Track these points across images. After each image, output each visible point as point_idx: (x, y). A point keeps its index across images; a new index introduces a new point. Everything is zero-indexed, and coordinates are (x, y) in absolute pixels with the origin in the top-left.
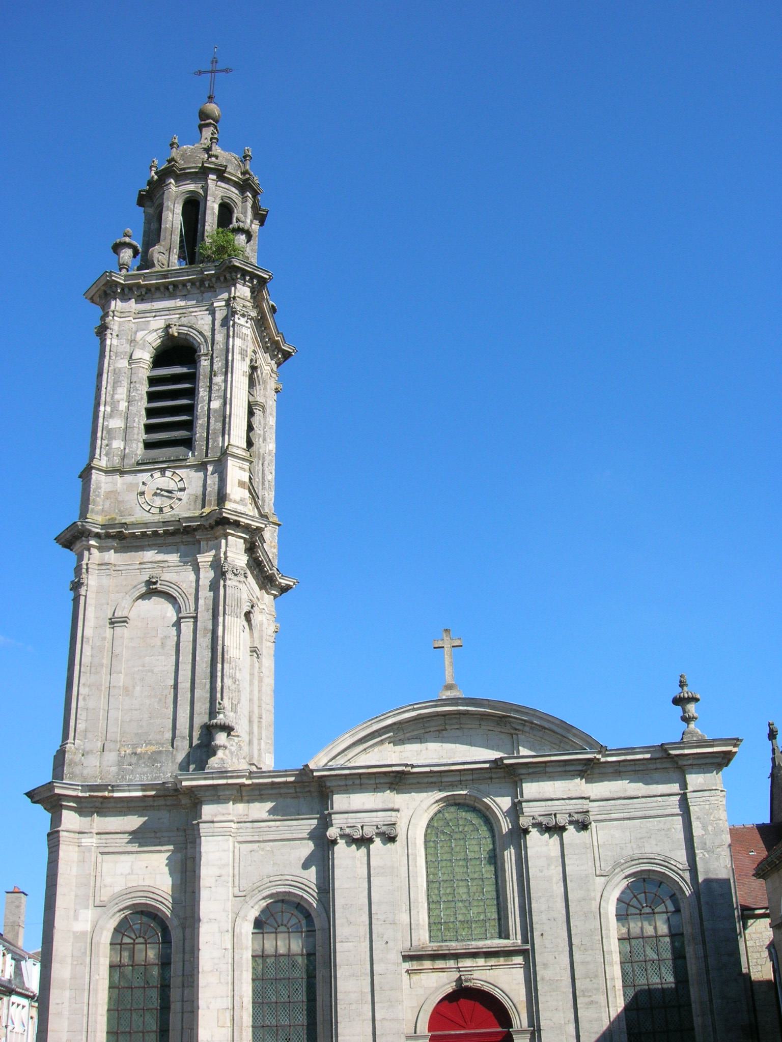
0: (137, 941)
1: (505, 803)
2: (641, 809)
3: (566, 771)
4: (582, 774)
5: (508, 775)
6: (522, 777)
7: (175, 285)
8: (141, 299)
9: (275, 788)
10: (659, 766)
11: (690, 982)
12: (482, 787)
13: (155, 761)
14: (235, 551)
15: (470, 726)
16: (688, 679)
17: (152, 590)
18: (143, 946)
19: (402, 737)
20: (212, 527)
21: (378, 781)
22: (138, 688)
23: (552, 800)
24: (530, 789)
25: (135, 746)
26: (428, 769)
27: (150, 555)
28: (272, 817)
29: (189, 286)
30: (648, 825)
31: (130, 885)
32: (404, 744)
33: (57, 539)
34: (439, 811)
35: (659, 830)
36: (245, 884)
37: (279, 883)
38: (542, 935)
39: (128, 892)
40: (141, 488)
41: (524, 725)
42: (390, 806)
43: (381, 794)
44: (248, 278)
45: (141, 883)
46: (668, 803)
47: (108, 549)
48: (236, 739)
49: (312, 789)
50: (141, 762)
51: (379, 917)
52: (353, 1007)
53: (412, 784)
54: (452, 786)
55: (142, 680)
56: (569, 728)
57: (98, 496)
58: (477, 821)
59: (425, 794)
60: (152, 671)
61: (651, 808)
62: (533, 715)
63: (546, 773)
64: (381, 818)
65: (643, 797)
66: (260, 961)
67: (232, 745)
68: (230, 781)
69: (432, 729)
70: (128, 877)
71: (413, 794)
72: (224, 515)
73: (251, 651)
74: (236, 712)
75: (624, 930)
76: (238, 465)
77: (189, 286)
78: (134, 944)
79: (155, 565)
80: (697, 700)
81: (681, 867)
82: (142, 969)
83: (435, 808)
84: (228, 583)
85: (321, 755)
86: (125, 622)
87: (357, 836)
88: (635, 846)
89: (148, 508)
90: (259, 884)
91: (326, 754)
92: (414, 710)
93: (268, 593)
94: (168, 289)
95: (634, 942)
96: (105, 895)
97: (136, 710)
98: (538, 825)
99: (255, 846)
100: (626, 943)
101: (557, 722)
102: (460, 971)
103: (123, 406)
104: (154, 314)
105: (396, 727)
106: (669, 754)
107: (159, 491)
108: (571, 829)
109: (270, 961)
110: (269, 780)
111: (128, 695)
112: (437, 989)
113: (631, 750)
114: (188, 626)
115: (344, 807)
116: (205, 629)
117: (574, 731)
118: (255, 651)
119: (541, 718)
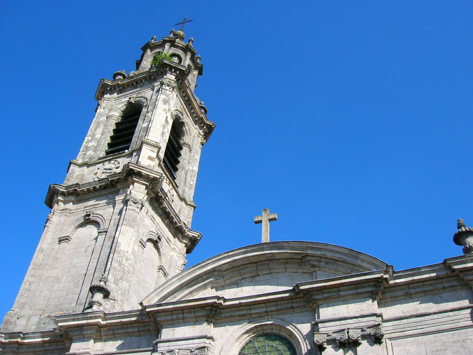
1: (306, 328)
3: (357, 294)
4: (373, 296)
5: (306, 302)
6: (320, 302)
8: (120, 92)
9: (124, 328)
10: (446, 285)
12: (286, 317)
14: (138, 191)
15: (277, 270)
17: (88, 221)
19: (223, 283)
21: (196, 314)
22: (65, 277)
23: (345, 319)
24: (326, 312)
26: (237, 302)
28: (119, 351)
30: (443, 338)
32: (224, 289)
34: (250, 342)
35: (454, 342)
41: (320, 261)
42: (204, 334)
43: (200, 326)
44: (173, 70)
46: (459, 317)
47: (69, 202)
48: (112, 301)
49: (151, 328)
53: (226, 317)
54: (260, 317)
56: (356, 254)
57: (72, 177)
58: (282, 347)
59: (237, 326)
62: (326, 250)
63: (340, 296)
65: (434, 313)
67: (107, 304)
68: (90, 321)
69: (247, 276)
71: (227, 326)
72: (130, 167)
73: (159, 269)
74: (117, 285)
76: (150, 149)
83: (246, 338)
84: (129, 207)
86: (67, 239)
92: (229, 257)
93: (181, 242)
98: (331, 342)
101: (347, 252)
105: (216, 273)
106: (454, 270)
107: (105, 171)
108: (364, 343)
110: (119, 320)
113: (416, 271)
114: (101, 237)
116: (111, 236)
117: (362, 257)
118: (161, 269)
119: (333, 251)
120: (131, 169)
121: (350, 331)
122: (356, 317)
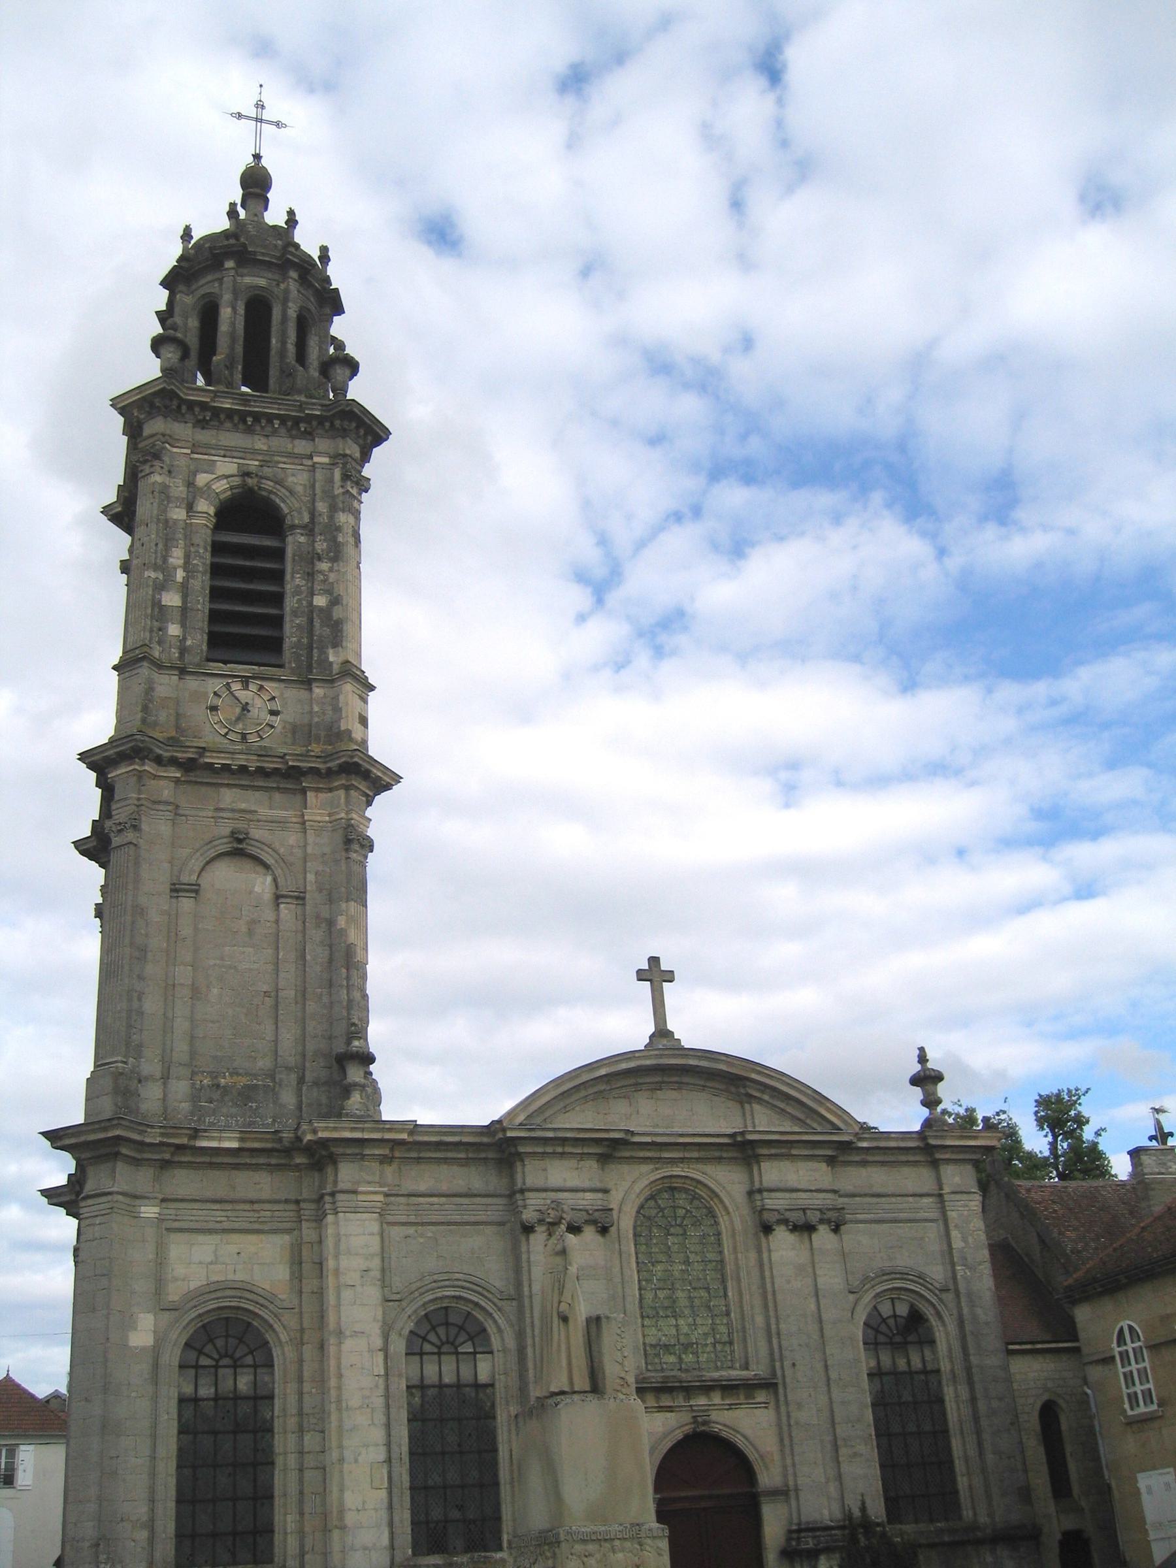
0: (221, 1363)
3: (211, 1163)
7: (257, 417)
11: (952, 1432)
17: (239, 849)
18: (230, 1371)
20: (330, 773)
22: (215, 991)
25: (214, 1075)
27: (229, 797)
29: (276, 423)
31: (214, 1278)
33: (84, 757)
36: (397, 1282)
37: (447, 1283)
38: (794, 1365)
39: (244, 1289)
45: (231, 1277)
50: (227, 1098)
61: (901, 1211)
64: (589, 1200)
66: (417, 1393)
75: (873, 1363)
77: (276, 423)
78: (216, 1367)
79: (237, 815)
81: (938, 1285)
89: (223, 731)
90: (418, 1284)
94: (245, 422)
95: (886, 1379)
96: (174, 1293)
97: (212, 1022)
99: (411, 1230)
100: (877, 1380)
101: (810, 1092)
102: (693, 1411)
103: (180, 575)
104: (222, 453)
106: (928, 1144)
109: (431, 1392)
112: (665, 1435)
115: (540, 1183)
120: (293, 767)
121: (808, 1212)
122: (811, 1191)
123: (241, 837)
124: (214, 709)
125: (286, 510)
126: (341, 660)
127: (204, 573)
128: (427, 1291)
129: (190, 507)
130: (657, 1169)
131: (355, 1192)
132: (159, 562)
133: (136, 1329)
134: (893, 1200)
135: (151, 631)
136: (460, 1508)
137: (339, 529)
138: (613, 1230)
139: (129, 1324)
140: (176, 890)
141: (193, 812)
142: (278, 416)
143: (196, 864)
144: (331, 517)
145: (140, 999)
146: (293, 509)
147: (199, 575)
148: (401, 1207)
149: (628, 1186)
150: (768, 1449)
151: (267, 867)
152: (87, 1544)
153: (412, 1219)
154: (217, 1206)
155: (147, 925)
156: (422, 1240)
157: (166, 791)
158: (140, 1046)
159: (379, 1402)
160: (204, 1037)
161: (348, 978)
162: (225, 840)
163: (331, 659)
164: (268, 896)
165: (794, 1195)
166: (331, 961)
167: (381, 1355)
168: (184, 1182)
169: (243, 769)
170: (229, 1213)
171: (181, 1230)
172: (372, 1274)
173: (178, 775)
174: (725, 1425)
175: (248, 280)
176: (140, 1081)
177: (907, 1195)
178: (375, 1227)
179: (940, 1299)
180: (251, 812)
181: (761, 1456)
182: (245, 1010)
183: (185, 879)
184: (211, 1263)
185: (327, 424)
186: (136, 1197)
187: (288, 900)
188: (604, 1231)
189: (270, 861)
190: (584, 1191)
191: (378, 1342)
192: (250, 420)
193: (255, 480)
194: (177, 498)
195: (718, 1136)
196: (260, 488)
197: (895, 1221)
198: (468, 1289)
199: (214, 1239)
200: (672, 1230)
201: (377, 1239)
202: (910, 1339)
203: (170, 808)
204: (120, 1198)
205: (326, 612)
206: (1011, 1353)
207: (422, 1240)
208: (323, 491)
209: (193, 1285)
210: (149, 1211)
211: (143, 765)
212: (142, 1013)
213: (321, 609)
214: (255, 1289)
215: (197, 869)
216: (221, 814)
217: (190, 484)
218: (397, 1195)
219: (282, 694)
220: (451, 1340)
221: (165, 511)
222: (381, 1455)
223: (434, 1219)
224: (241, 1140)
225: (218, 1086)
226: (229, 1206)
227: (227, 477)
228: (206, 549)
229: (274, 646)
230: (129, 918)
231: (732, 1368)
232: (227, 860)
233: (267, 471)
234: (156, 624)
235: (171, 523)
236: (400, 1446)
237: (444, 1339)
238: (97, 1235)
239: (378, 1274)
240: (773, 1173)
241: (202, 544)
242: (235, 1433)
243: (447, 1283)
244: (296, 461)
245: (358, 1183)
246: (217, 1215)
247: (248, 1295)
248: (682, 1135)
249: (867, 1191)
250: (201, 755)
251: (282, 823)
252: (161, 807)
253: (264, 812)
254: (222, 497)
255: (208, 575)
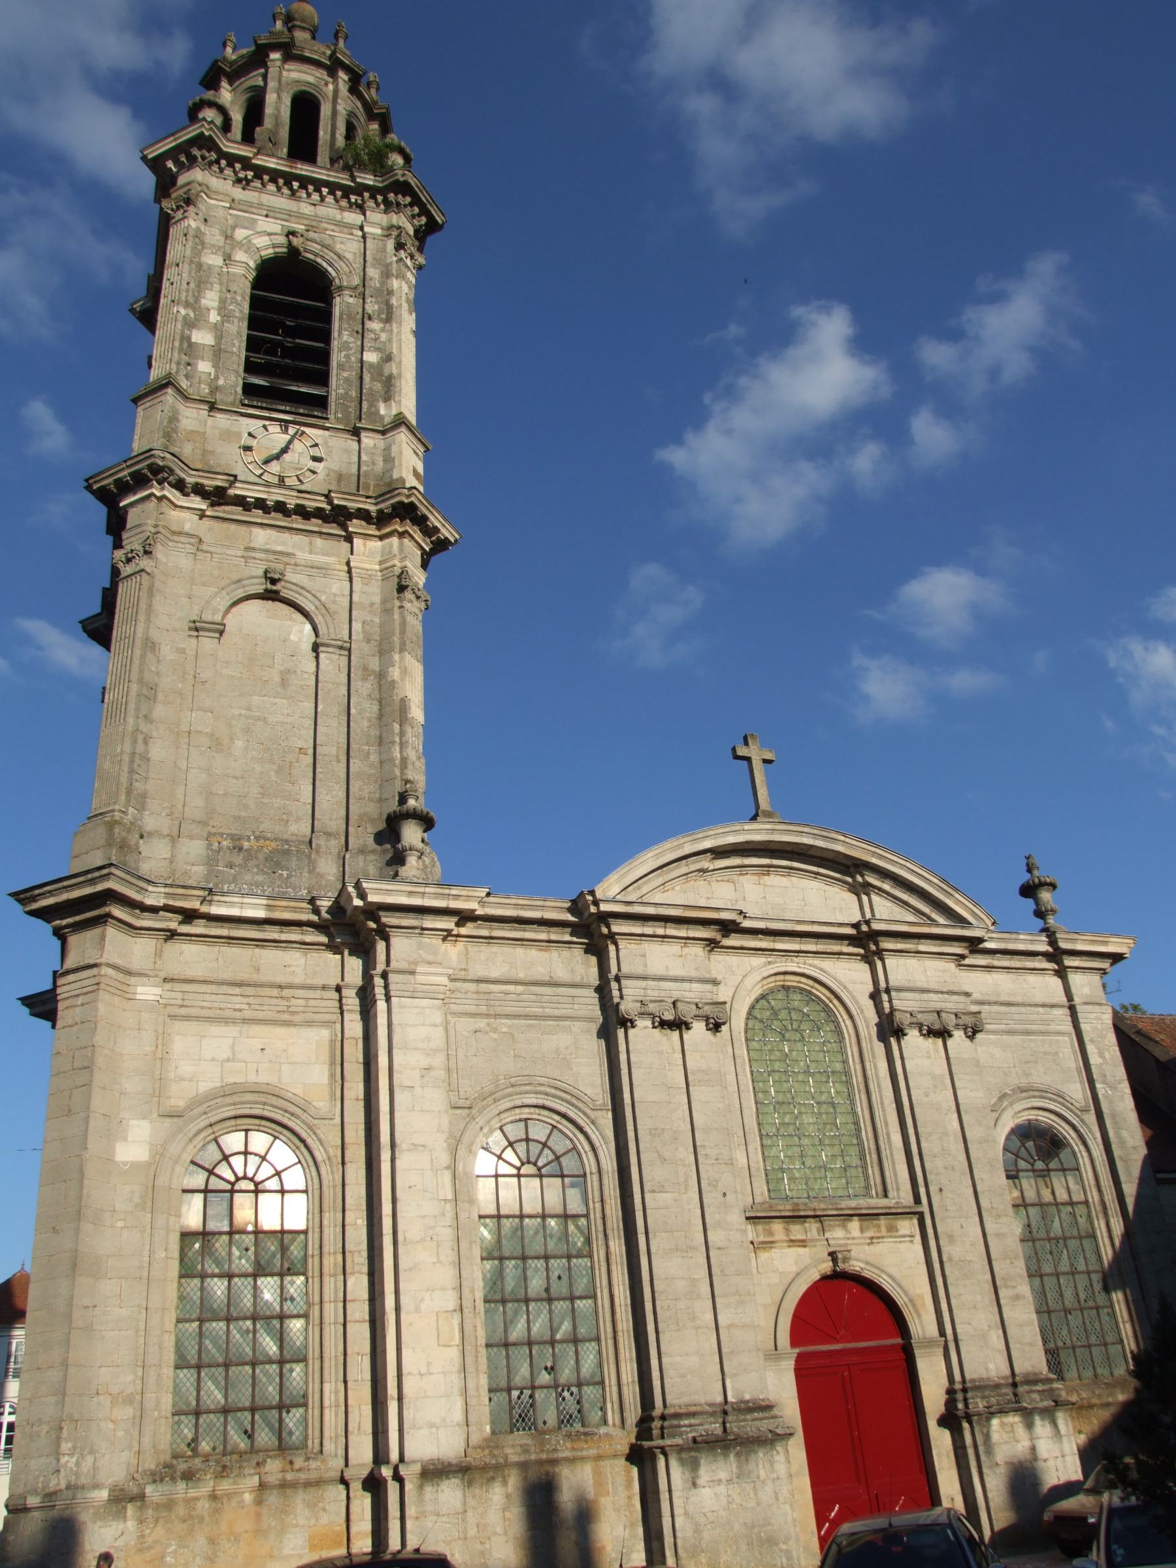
2: (1021, 1022)
13: (278, 865)
16: (1036, 861)
17: (272, 592)
22: (239, 744)
27: (261, 537)
31: (231, 1080)
37: (527, 1088)
38: (941, 1190)
40: (245, 440)
45: (252, 1078)
50: (251, 864)
51: (708, 1151)
52: (682, 1305)
55: (247, 730)
60: (265, 720)
61: (1031, 1022)
70: (225, 1064)
75: (1016, 1194)
78: (232, 1192)
80: (1053, 886)
81: (1077, 1105)
82: (249, 1240)
85: (613, 877)
87: (669, 1016)
88: (1020, 1073)
89: (258, 472)
91: (618, 881)
96: (178, 1098)
97: (235, 777)
98: (920, 1026)
99: (481, 1023)
111: (219, 751)
120: (339, 506)
122: (942, 992)
123: (277, 576)
124: (248, 449)
125: (334, 274)
126: (394, 412)
127: (240, 319)
128: (504, 1097)
129: (228, 258)
130: (770, 963)
131: (413, 973)
132: (191, 300)
133: (126, 1139)
134: (1023, 1009)
135: (178, 364)
136: (551, 1370)
137: (390, 293)
138: (724, 1028)
139: (115, 1131)
140: (196, 628)
141: (219, 550)
142: (327, 184)
143: (223, 602)
144: (383, 283)
145: (146, 742)
146: (343, 273)
147: (236, 321)
148: (469, 995)
149: (741, 976)
150: (918, 1292)
151: (306, 614)
152: (45, 1428)
153: (483, 1009)
154: (237, 990)
155: (159, 661)
156: (495, 1036)
157: (188, 522)
158: (144, 796)
159: (446, 1234)
160: (225, 795)
161: (402, 734)
162: (257, 581)
163: (382, 412)
164: (307, 646)
165: (925, 996)
166: (381, 716)
167: (447, 1176)
168: (191, 957)
169: (280, 507)
170: (251, 1000)
171: (188, 1018)
172: (433, 1073)
173: (204, 507)
174: (867, 1263)
175: (295, 75)
176: (142, 837)
177: (1037, 1005)
178: (438, 1017)
179: (1082, 1120)
180: (288, 554)
181: (911, 1300)
182: (275, 767)
183: (207, 617)
184: (228, 1060)
185: (380, 198)
186: (129, 973)
187: (330, 650)
188: (716, 1027)
189: (309, 607)
190: (690, 981)
191: (444, 1159)
192: (296, 185)
193: (301, 240)
194: (213, 246)
195: (841, 925)
196: (306, 250)
197: (1028, 1033)
198: (554, 1096)
199: (232, 1031)
200: (787, 1035)
201: (441, 1030)
202: (1052, 1165)
203: (192, 540)
204: (110, 971)
205: (377, 370)
206: (1160, 1182)
207: (495, 1036)
208: (374, 259)
209: (204, 1087)
210: (147, 992)
211: (163, 489)
212: (148, 760)
213: (371, 365)
214: (282, 1093)
215: (223, 609)
216: (253, 554)
217: (228, 237)
218: (464, 980)
219: (326, 443)
220: (533, 1159)
221: (199, 254)
222: (451, 1302)
223: (509, 1010)
224: (269, 907)
225: (241, 849)
226: (250, 991)
227: (270, 234)
228: (244, 298)
229: (321, 403)
230: (138, 652)
231: (867, 1194)
232: (257, 603)
233: (312, 235)
234: (185, 358)
235: (205, 267)
236: (472, 1291)
237: (524, 1156)
238: (78, 1019)
239: (442, 1074)
240: (901, 969)
241: (239, 292)
242: (255, 1276)
243: (527, 1088)
244: (346, 230)
245: (416, 963)
246: (237, 1001)
247: (275, 1101)
248: (799, 922)
249: (993, 998)
250: (232, 484)
251: (323, 570)
252: (182, 539)
253: (303, 556)
254: (263, 253)
255: (246, 324)
